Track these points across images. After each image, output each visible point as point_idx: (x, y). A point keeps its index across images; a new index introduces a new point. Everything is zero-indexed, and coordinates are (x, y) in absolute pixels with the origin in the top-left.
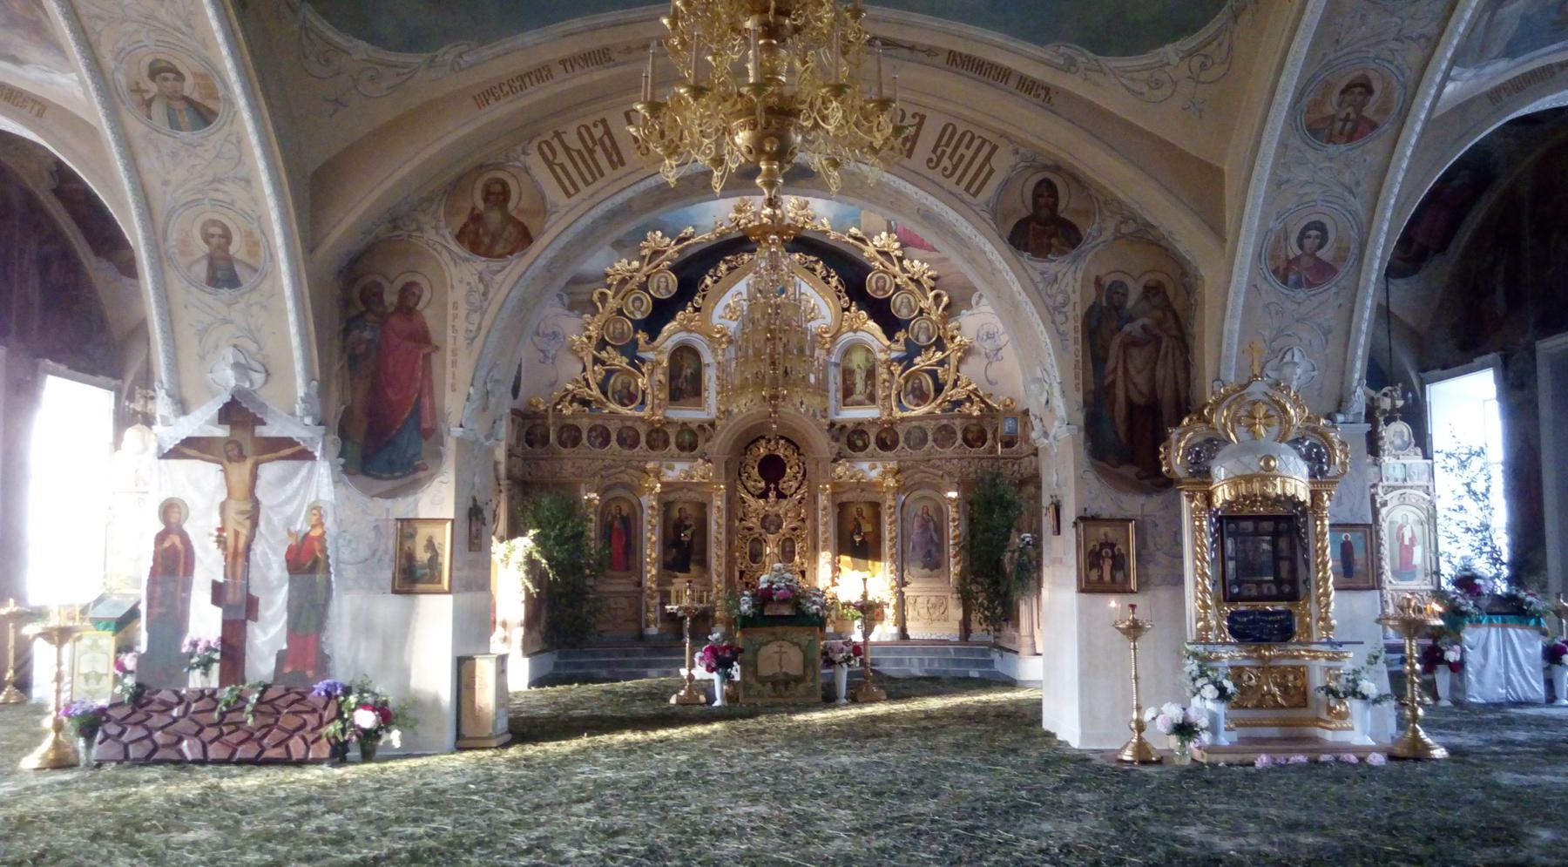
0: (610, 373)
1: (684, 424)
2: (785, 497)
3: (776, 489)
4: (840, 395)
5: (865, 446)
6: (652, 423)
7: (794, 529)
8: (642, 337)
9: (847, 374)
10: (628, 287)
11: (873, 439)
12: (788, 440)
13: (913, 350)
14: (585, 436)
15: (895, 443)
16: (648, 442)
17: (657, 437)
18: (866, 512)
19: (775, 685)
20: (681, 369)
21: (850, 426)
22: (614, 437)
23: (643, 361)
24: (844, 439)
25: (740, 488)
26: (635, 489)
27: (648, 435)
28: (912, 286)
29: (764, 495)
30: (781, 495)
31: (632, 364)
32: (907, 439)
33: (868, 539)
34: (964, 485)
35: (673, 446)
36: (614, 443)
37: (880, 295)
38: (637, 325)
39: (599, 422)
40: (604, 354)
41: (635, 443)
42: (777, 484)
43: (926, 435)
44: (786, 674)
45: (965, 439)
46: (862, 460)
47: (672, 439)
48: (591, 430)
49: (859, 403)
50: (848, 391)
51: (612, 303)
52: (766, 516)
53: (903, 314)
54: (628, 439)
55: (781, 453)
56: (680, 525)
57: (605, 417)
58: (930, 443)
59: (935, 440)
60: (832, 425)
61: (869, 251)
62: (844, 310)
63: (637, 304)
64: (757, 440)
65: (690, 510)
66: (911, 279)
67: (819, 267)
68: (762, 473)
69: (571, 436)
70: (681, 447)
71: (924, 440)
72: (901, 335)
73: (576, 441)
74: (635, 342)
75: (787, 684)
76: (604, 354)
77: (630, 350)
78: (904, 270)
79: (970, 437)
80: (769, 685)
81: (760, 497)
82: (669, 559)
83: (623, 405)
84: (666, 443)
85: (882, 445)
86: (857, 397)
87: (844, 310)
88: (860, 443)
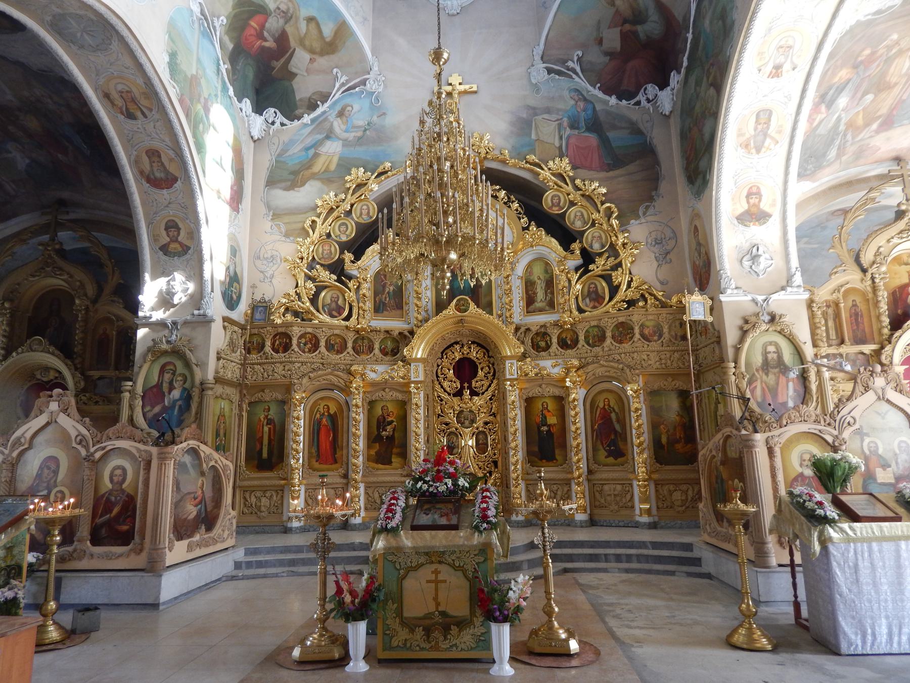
0: (319, 290)
1: (387, 332)
2: (477, 394)
3: (470, 387)
4: (523, 304)
5: (548, 347)
6: (357, 331)
7: (486, 423)
8: (348, 256)
9: (529, 285)
10: (335, 214)
11: (555, 340)
12: (479, 345)
13: (588, 257)
14: (295, 341)
15: (575, 342)
16: (354, 348)
17: (363, 343)
18: (551, 406)
19: (428, 631)
20: (384, 286)
21: (534, 329)
22: (322, 343)
23: (350, 278)
24: (528, 341)
25: (437, 387)
26: (346, 390)
27: (355, 342)
28: (585, 203)
29: (459, 394)
30: (474, 393)
31: (339, 280)
32: (586, 338)
33: (554, 430)
34: (569, 118)
35: (377, 351)
36: (322, 349)
37: (556, 211)
38: (344, 247)
39: (309, 330)
40: (314, 272)
41: (343, 348)
42: (470, 384)
43: (604, 333)
44: (443, 614)
45: (642, 335)
46: (543, 358)
47: (377, 346)
48: (300, 337)
49: (541, 310)
50: (530, 300)
51: (321, 229)
52: (461, 412)
53: (578, 225)
54: (337, 345)
55: (458, 356)
56: (382, 423)
57: (315, 327)
58: (609, 341)
59: (613, 337)
60: (517, 329)
61: (545, 174)
62: (524, 229)
63: (343, 228)
64: (452, 345)
65: (391, 407)
66: (583, 195)
67: (503, 193)
68: (457, 374)
69: (283, 342)
70: (384, 352)
71: (602, 338)
72: (576, 246)
73: (287, 347)
74: (341, 262)
75: (446, 629)
76: (314, 272)
77: (337, 268)
78: (577, 188)
79: (646, 332)
80: (420, 632)
81: (454, 395)
82: (373, 452)
83: (332, 316)
84: (371, 349)
85: (563, 344)
86: (538, 305)
87: (524, 229)
88: (543, 344)
